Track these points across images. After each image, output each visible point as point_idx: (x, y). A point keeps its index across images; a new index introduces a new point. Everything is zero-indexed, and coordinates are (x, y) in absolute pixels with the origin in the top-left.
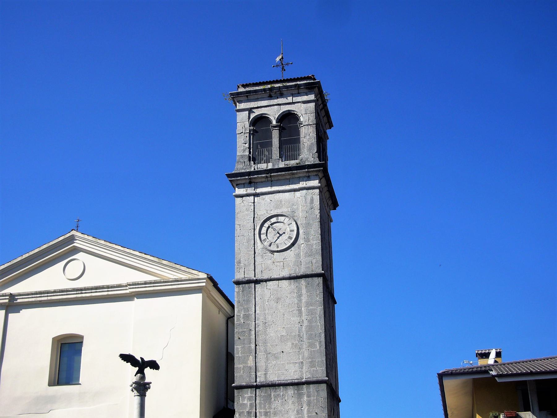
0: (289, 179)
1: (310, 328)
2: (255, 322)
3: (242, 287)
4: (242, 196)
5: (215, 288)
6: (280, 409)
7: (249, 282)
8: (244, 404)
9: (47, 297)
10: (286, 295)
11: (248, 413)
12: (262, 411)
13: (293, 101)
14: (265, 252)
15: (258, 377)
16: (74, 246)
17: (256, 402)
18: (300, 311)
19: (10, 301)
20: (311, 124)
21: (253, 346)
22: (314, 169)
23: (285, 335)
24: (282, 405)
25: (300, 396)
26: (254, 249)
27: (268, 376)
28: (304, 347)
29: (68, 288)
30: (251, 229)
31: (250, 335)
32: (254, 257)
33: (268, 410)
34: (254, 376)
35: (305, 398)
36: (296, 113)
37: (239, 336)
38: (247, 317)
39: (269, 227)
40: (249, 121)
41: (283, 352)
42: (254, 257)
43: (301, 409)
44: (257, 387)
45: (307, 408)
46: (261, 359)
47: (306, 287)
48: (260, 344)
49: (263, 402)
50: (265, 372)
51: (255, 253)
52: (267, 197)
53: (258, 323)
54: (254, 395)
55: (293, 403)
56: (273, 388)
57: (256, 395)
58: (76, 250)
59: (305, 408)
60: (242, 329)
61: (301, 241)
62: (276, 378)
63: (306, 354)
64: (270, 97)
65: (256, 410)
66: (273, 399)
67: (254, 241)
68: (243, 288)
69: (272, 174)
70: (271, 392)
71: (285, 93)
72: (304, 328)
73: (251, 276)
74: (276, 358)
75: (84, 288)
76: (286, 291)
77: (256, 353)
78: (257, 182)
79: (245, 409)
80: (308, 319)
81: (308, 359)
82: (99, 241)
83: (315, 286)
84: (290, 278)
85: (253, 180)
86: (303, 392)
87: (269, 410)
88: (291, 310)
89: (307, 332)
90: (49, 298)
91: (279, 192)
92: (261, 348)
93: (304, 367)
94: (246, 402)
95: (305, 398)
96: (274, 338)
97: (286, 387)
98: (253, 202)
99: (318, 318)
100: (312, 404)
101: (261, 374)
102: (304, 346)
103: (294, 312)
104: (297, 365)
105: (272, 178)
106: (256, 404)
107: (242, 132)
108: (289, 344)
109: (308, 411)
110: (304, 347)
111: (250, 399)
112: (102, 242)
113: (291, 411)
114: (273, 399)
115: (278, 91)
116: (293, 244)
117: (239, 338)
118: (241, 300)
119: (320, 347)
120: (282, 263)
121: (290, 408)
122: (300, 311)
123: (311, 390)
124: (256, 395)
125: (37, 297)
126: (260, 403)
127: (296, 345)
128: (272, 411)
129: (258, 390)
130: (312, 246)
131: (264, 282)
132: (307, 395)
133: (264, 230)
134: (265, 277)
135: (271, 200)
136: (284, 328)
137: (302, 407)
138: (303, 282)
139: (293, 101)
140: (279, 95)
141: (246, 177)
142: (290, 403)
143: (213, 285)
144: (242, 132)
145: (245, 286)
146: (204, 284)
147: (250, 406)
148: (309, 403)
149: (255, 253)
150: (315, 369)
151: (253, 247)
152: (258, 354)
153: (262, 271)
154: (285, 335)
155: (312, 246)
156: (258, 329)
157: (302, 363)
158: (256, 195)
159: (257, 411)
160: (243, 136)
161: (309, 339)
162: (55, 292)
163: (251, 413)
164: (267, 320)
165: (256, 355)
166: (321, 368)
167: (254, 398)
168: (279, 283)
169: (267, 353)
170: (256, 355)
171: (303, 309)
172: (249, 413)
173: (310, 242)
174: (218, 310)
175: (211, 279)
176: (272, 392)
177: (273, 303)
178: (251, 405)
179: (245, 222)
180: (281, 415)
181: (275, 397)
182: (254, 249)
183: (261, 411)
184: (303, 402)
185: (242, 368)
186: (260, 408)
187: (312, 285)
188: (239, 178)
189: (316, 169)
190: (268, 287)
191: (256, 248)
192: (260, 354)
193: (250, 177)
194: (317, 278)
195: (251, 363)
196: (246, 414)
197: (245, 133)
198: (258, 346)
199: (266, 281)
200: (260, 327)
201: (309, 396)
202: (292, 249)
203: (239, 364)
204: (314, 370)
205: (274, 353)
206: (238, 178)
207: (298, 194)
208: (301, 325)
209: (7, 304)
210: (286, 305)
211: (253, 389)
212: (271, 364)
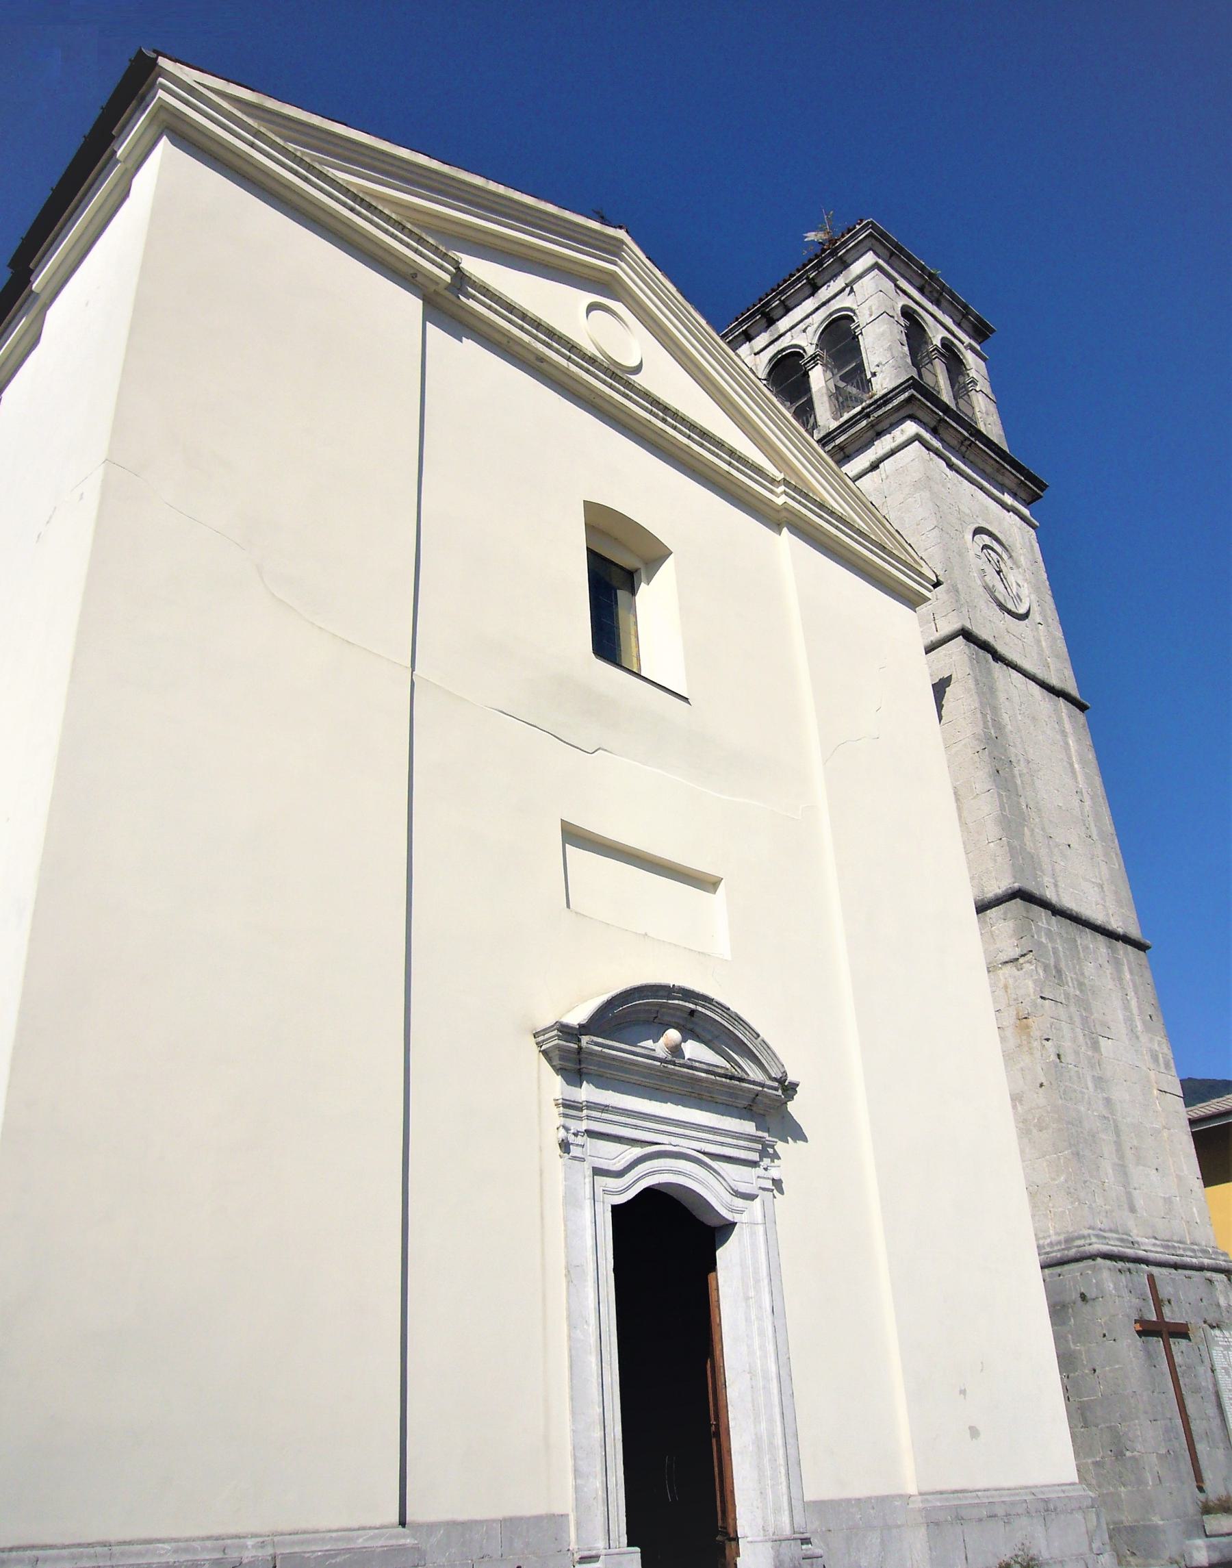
16: (613, 275)
105: (968, 452)
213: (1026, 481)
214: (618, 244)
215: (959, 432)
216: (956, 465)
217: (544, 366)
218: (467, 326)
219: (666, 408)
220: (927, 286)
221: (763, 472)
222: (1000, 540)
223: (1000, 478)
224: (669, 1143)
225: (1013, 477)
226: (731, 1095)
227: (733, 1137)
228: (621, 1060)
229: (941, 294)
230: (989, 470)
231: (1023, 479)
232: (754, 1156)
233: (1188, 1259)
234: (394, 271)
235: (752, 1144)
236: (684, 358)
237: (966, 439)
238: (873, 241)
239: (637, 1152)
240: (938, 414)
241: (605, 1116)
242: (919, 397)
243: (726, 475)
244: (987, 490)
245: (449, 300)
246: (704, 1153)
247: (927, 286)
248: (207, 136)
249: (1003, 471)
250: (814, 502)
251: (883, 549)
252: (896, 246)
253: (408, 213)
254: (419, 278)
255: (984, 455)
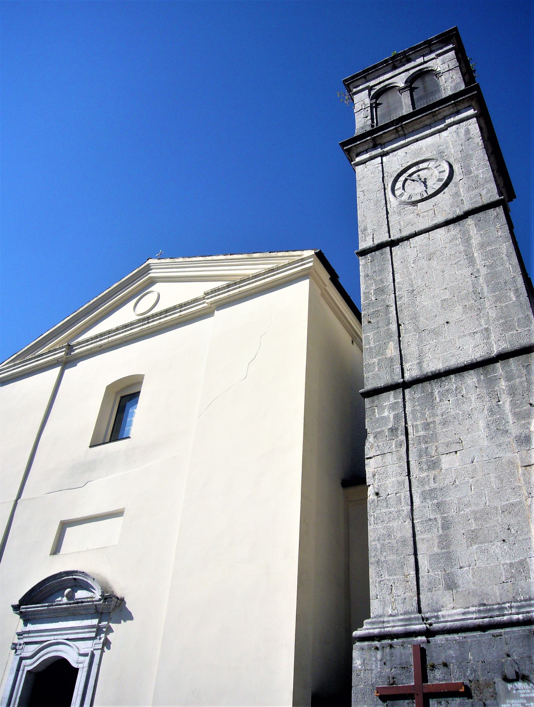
0: (430, 125)
1: (493, 276)
2: (395, 293)
3: (370, 256)
4: (364, 162)
5: (334, 287)
6: (453, 413)
7: (380, 246)
8: (384, 418)
9: (108, 339)
10: (443, 246)
11: (392, 431)
12: (418, 423)
13: (425, 61)
14: (403, 208)
15: (405, 370)
16: (151, 278)
17: (405, 410)
18: (471, 261)
19: (67, 354)
20: (453, 68)
21: (394, 327)
22: (464, 97)
23: (448, 298)
24: (457, 404)
25: (491, 382)
26: (387, 209)
27: (425, 365)
28: (486, 306)
29: (133, 320)
30: (379, 190)
31: (387, 312)
32: (387, 218)
33: (429, 420)
34: (399, 370)
35: (503, 384)
36: (430, 69)
37: (369, 320)
38: (381, 291)
39: (406, 180)
40: (369, 97)
41: (447, 323)
42: (387, 218)
43: (498, 405)
44: (405, 385)
45: (508, 400)
46: (409, 343)
47: (476, 225)
48: (407, 322)
49: (418, 408)
50: (419, 361)
51: (387, 213)
52: (400, 152)
53: (400, 294)
54: (400, 400)
55: (480, 397)
56: (436, 380)
57: (404, 399)
58: (152, 282)
59: (506, 402)
60: (373, 308)
61: (457, 177)
62: (440, 365)
63: (493, 314)
64: (395, 68)
65: (406, 423)
66: (438, 400)
67: (386, 201)
68: (373, 257)
69: (404, 123)
70: (432, 389)
71: (412, 57)
72: (481, 280)
73: (385, 238)
74: (436, 333)
75: (151, 315)
76: (442, 241)
77: (399, 336)
78: (385, 143)
79: (386, 425)
80: (488, 264)
81: (498, 320)
82: (176, 260)
83: (491, 220)
84: (447, 223)
85: (379, 141)
86: (496, 376)
87: (432, 420)
88: (454, 263)
89: (488, 283)
90: (110, 339)
91: (417, 140)
92: (407, 327)
93: (493, 335)
94: (386, 414)
95: (503, 384)
96: (430, 308)
97: (461, 373)
98: (381, 162)
99: (505, 258)
100: (520, 391)
101: (411, 365)
102: (487, 304)
103: (461, 263)
104: (477, 336)
105: (405, 131)
106: (405, 414)
107: (362, 109)
108: (459, 308)
109: (513, 404)
110: (486, 306)
111: (393, 407)
112: (181, 260)
113: (476, 413)
114: (438, 400)
115: (403, 58)
116: (446, 185)
117: (370, 322)
118: (369, 272)
119: (518, 297)
120: (431, 212)
121: (473, 407)
122: (471, 261)
123: (513, 367)
124: (404, 399)
125: (97, 342)
126: (413, 412)
127: (471, 308)
128: (438, 419)
129: (407, 391)
130: (477, 176)
131: (405, 240)
132: (507, 377)
133: (399, 184)
134: (405, 234)
135: (406, 153)
136: (446, 288)
137: (499, 401)
138: (470, 221)
139: (425, 61)
140: (405, 62)
141: (368, 138)
142: (473, 399)
143: (330, 278)
144: (362, 109)
145: (375, 254)
146: (311, 264)
147: (394, 418)
148: (512, 392)
149: (387, 213)
150: (515, 332)
151: (385, 208)
152: (403, 337)
153: (400, 230)
154: (448, 298)
155: (477, 176)
156: (400, 302)
157: (487, 330)
158: (382, 155)
159: (409, 423)
160: (363, 112)
161: (494, 291)
162: (117, 329)
163: (397, 429)
164: (415, 286)
165: (399, 339)
166: (526, 329)
167: (401, 405)
168: (429, 235)
169: (420, 331)
170: (399, 339)
171: (475, 255)
172: (394, 431)
173: (473, 173)
174: (351, 338)
175: (320, 255)
176: (435, 388)
177: (423, 263)
178: (396, 417)
179: (371, 186)
180: (456, 423)
181: (442, 394)
182: (387, 209)
183: (417, 425)
184: (500, 392)
185: (377, 363)
186: (415, 418)
187: (485, 221)
188: (358, 142)
189: (467, 96)
190: (412, 245)
191: (388, 207)
192: (408, 335)
193: (373, 137)
194: (492, 210)
195: (392, 351)
196: (387, 433)
197: (365, 108)
198: (403, 325)
199: (408, 238)
200: (403, 298)
201: (509, 379)
202: (446, 190)
203: (372, 357)
204: (512, 335)
205: (432, 327)
206: (356, 144)
207: (444, 134)
208: (476, 277)
209: (64, 359)
210: (444, 259)
211: (398, 390)
212: (428, 347)
213: (457, 100)
214: (148, 266)
215: (389, 131)
216: (388, 150)
217: (103, 347)
218: (81, 358)
219: (148, 318)
220: (395, 63)
221: (197, 299)
222: (425, 159)
223: (440, 117)
224: (52, 639)
225: (447, 108)
226: (84, 610)
227: (82, 629)
228: (34, 611)
229: (406, 56)
230: (427, 122)
231: (453, 102)
232: (93, 635)
233: (497, 619)
234: (256, 293)
235: (91, 629)
236: (181, 279)
237: (396, 129)
238: (352, 84)
239: (36, 647)
240: (369, 139)
241: (30, 635)
242: (350, 146)
243: (180, 317)
244: (419, 138)
245: (69, 357)
246: (68, 639)
247: (395, 63)
248: (224, 299)
249: (437, 112)
250: (264, 274)
251: (272, 270)
252: (364, 72)
253: (62, 342)
254: (59, 360)
255: (414, 122)
